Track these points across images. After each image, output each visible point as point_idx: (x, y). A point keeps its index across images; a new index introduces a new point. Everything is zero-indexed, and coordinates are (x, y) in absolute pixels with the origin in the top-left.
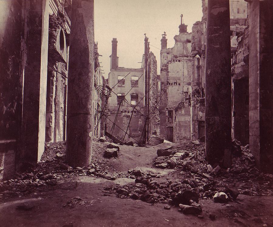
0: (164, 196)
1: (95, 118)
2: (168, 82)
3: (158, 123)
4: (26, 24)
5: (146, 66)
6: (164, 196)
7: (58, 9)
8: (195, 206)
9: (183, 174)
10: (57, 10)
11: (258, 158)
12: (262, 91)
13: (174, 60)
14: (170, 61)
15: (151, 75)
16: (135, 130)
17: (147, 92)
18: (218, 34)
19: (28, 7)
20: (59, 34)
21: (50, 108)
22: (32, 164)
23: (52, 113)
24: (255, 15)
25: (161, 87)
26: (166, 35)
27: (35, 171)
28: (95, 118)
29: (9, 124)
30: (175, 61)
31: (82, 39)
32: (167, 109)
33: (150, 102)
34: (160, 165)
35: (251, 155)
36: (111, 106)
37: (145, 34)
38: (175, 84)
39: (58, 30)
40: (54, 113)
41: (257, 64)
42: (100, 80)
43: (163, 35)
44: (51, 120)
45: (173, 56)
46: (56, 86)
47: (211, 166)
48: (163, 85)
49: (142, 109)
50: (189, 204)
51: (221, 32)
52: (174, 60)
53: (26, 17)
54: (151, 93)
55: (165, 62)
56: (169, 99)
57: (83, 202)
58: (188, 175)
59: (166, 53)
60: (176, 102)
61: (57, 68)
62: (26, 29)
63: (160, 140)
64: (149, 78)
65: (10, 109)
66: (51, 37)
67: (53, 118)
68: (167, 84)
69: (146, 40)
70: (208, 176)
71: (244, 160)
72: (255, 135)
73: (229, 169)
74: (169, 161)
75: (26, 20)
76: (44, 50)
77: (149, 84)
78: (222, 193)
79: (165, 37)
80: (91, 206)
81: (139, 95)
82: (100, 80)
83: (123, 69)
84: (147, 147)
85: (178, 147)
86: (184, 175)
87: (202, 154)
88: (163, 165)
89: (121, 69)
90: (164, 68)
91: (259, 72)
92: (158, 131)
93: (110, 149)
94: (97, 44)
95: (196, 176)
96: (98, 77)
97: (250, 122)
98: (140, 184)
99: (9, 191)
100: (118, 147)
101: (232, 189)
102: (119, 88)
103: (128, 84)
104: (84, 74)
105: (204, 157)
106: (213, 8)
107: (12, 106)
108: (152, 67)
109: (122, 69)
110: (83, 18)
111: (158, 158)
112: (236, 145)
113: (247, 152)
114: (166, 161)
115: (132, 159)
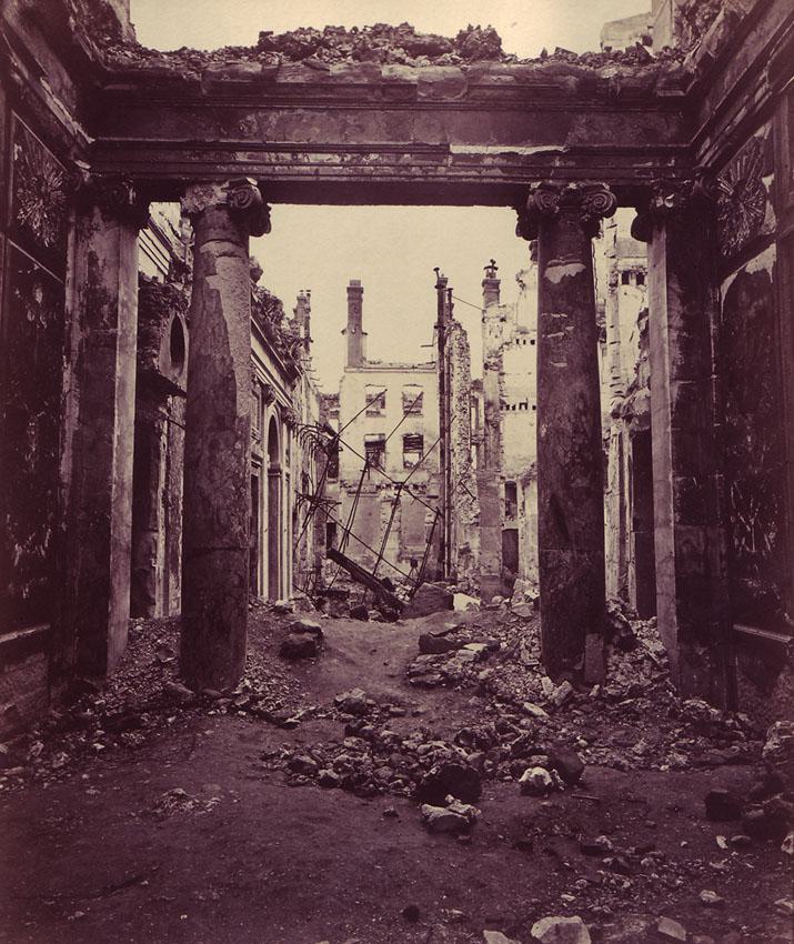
0: (405, 777)
1: (295, 515)
2: (503, 402)
3: (476, 520)
4: (76, 325)
5: (441, 360)
6: (405, 777)
7: (172, 254)
8: (455, 812)
9: (475, 706)
10: (168, 258)
11: (674, 653)
12: (679, 479)
13: (518, 341)
14: (507, 344)
15: (455, 384)
16: (416, 539)
17: (445, 430)
18: (563, 334)
19: (83, 279)
20: (168, 331)
21: (151, 519)
22: (94, 684)
23: (157, 531)
24: (659, 280)
25: (486, 415)
26: (496, 269)
27: (97, 703)
28: (295, 515)
29: (30, 587)
30: (521, 342)
31: (218, 356)
32: (502, 478)
33: (453, 461)
34: (420, 679)
35: (659, 647)
36: (349, 473)
37: (437, 269)
38: (523, 407)
39: (164, 321)
40: (162, 532)
41: (665, 406)
42: (309, 407)
43: (489, 267)
44: (154, 552)
45: (515, 328)
46: (168, 458)
47: (550, 681)
48: (491, 409)
49: (433, 480)
50: (445, 804)
51: (570, 328)
52: (518, 341)
53: (76, 306)
54: (455, 434)
55: (496, 344)
56: (506, 450)
57: (190, 803)
58: (488, 708)
59: (498, 319)
60: (525, 458)
61: (169, 411)
62: (77, 337)
63: (443, 598)
64: (450, 393)
65: (32, 548)
66: (146, 340)
67: (161, 545)
68: (502, 408)
69: (441, 285)
70: (537, 710)
71: (641, 662)
72: (667, 595)
73: (597, 687)
74: (444, 668)
75: (77, 315)
76: (123, 384)
77: (448, 412)
78: (539, 771)
79: (491, 275)
80: (212, 814)
81: (425, 439)
82: (309, 407)
83: (377, 366)
84: (399, 624)
85: (474, 626)
86: (479, 706)
87: (533, 645)
88: (428, 679)
89: (373, 366)
90: (493, 360)
91: (669, 429)
92: (475, 543)
93: (298, 636)
94: (309, 295)
95: (508, 711)
96: (304, 401)
97: (658, 559)
98: (354, 740)
99: (24, 766)
100: (317, 630)
101: (563, 759)
102: (371, 420)
103: (394, 408)
104: (222, 446)
105: (538, 655)
106: (551, 266)
107: (39, 541)
108: (456, 364)
109: (377, 366)
110: (220, 300)
111: (419, 659)
112: (621, 622)
113: (650, 637)
114: (438, 667)
115: (353, 663)
